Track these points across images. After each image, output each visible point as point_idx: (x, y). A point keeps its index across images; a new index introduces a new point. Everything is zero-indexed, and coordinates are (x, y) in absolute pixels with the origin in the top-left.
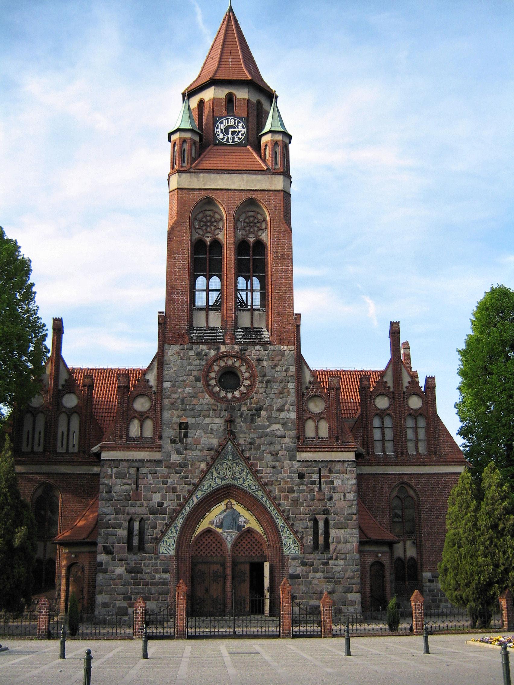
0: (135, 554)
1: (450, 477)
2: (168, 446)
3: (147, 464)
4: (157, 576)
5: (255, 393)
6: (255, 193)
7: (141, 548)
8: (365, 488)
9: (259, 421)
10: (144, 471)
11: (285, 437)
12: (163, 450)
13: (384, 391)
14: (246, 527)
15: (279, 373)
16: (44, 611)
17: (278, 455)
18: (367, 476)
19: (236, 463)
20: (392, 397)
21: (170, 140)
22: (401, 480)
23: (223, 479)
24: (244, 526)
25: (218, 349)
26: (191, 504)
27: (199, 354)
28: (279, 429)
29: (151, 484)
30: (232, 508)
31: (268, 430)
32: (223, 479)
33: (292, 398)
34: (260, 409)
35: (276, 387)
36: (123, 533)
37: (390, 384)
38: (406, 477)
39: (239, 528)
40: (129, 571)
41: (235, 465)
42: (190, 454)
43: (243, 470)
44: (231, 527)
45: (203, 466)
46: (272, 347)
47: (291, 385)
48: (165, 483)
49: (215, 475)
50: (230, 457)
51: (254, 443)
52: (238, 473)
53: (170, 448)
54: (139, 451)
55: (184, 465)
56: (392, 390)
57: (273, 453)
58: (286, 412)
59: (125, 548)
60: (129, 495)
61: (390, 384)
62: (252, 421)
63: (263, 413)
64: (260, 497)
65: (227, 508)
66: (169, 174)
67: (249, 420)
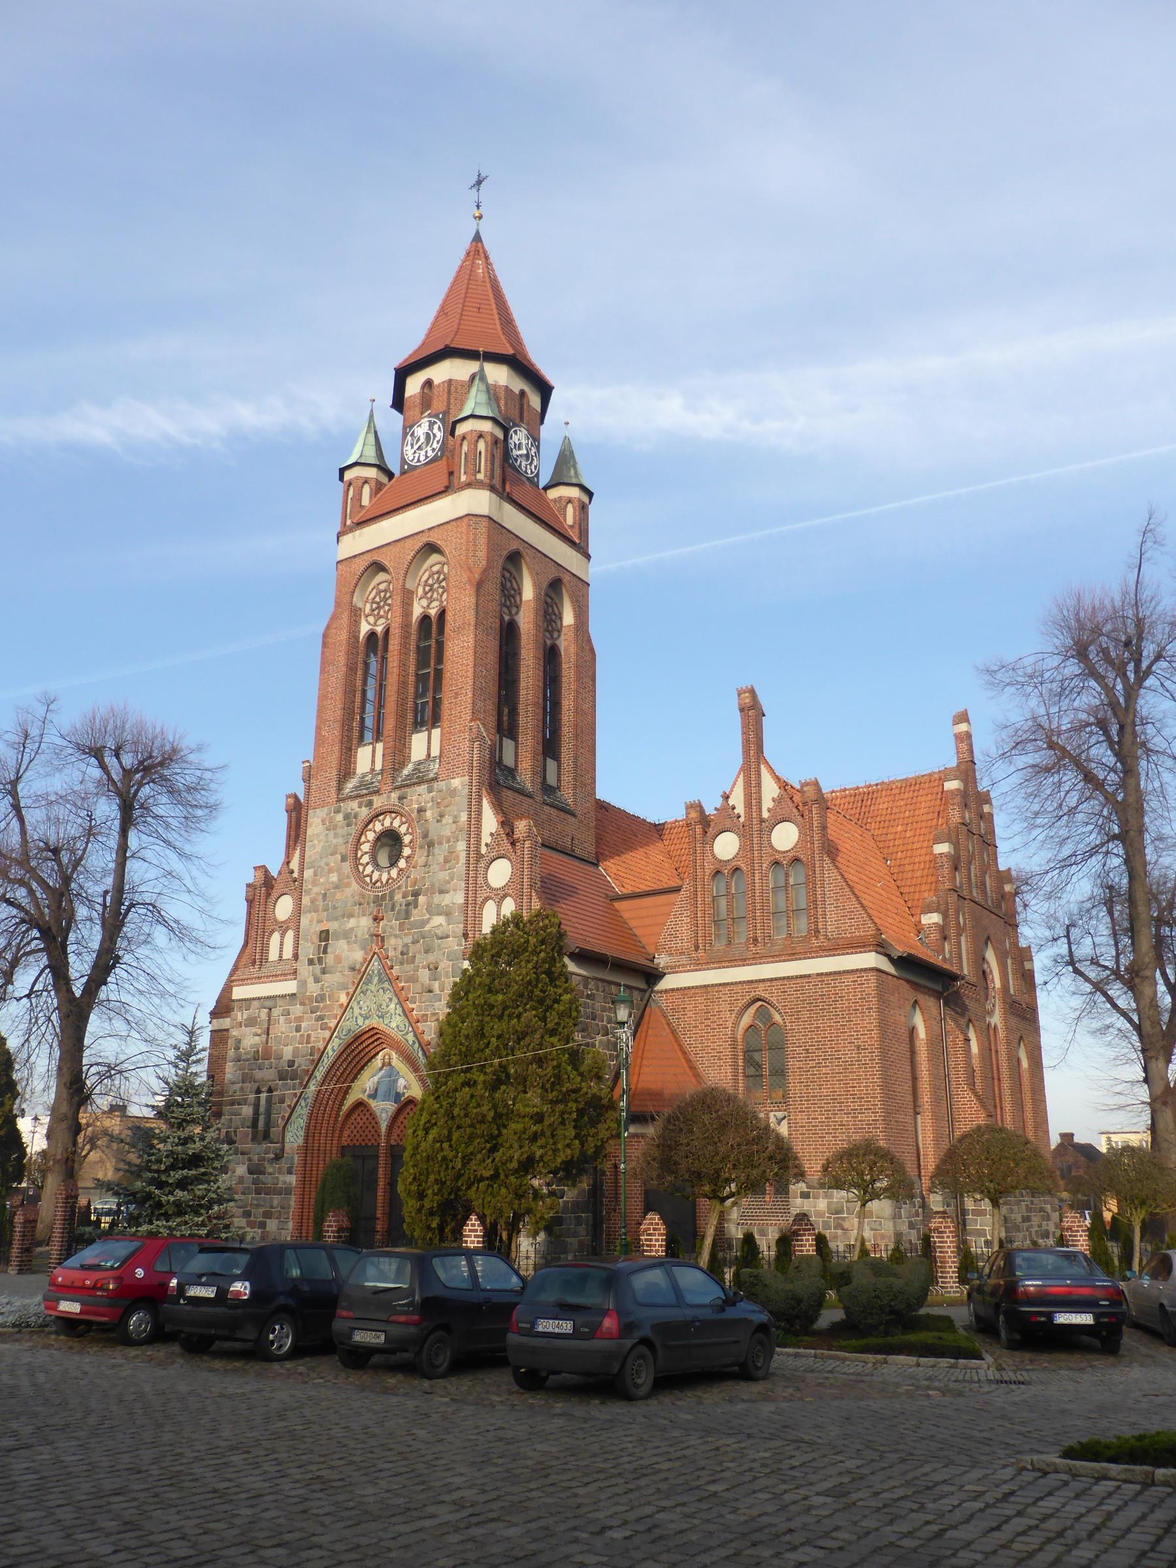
0: (259, 1144)
1: (844, 978)
2: (304, 970)
3: (279, 1002)
4: (281, 1178)
5: (414, 867)
6: (431, 533)
7: (266, 1136)
8: (690, 1014)
9: (416, 915)
10: (276, 1012)
11: (448, 937)
12: (298, 977)
13: (728, 823)
14: (406, 1095)
15: (447, 828)
16: (473, 1239)
17: (437, 968)
18: (693, 991)
19: (383, 988)
20: (745, 832)
21: (341, 478)
22: (753, 994)
23: (366, 1018)
24: (404, 1093)
25: (370, 804)
26: (326, 1060)
27: (347, 817)
28: (441, 925)
29: (282, 1033)
30: (390, 1064)
31: (427, 928)
32: (366, 1018)
33: (460, 866)
34: (416, 894)
35: (440, 852)
36: (247, 1111)
37: (740, 809)
38: (761, 986)
39: (398, 1096)
40: (250, 1172)
41: (381, 991)
42: (331, 979)
43: (391, 1000)
44: (386, 1098)
45: (343, 999)
46: (441, 785)
47: (461, 846)
48: (298, 1029)
49: (357, 1011)
50: (376, 980)
51: (407, 953)
52: (384, 1006)
53: (306, 974)
54: (834, 955)
55: (321, 998)
56: (742, 819)
57: (431, 967)
58: (452, 892)
59: (248, 1136)
60: (258, 1051)
61: (740, 809)
62: (407, 915)
63: (421, 899)
64: (411, 1043)
65: (383, 1065)
66: (339, 533)
67: (403, 914)
